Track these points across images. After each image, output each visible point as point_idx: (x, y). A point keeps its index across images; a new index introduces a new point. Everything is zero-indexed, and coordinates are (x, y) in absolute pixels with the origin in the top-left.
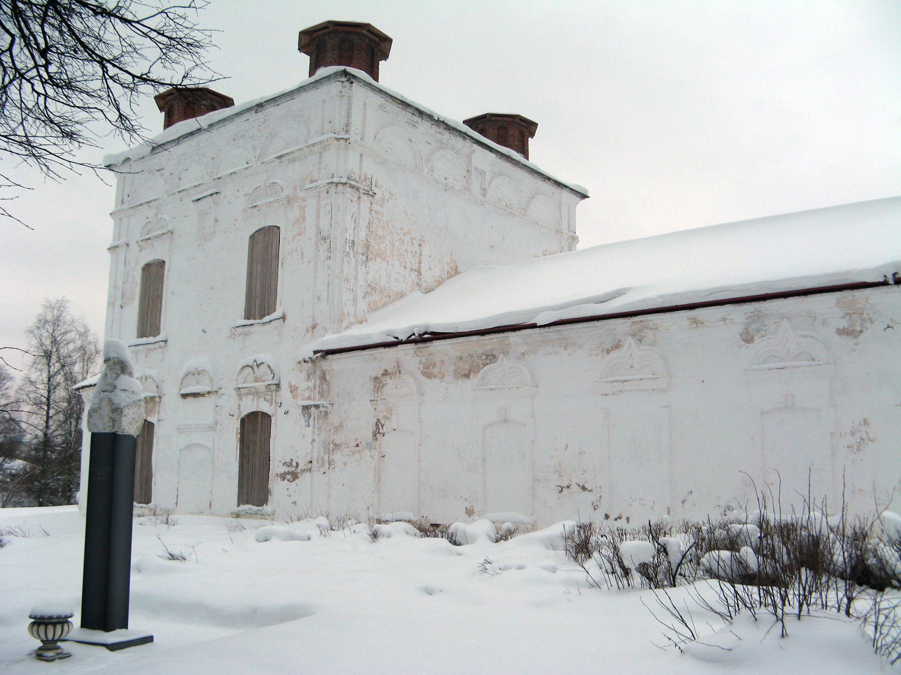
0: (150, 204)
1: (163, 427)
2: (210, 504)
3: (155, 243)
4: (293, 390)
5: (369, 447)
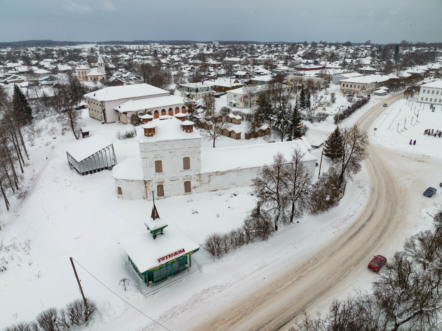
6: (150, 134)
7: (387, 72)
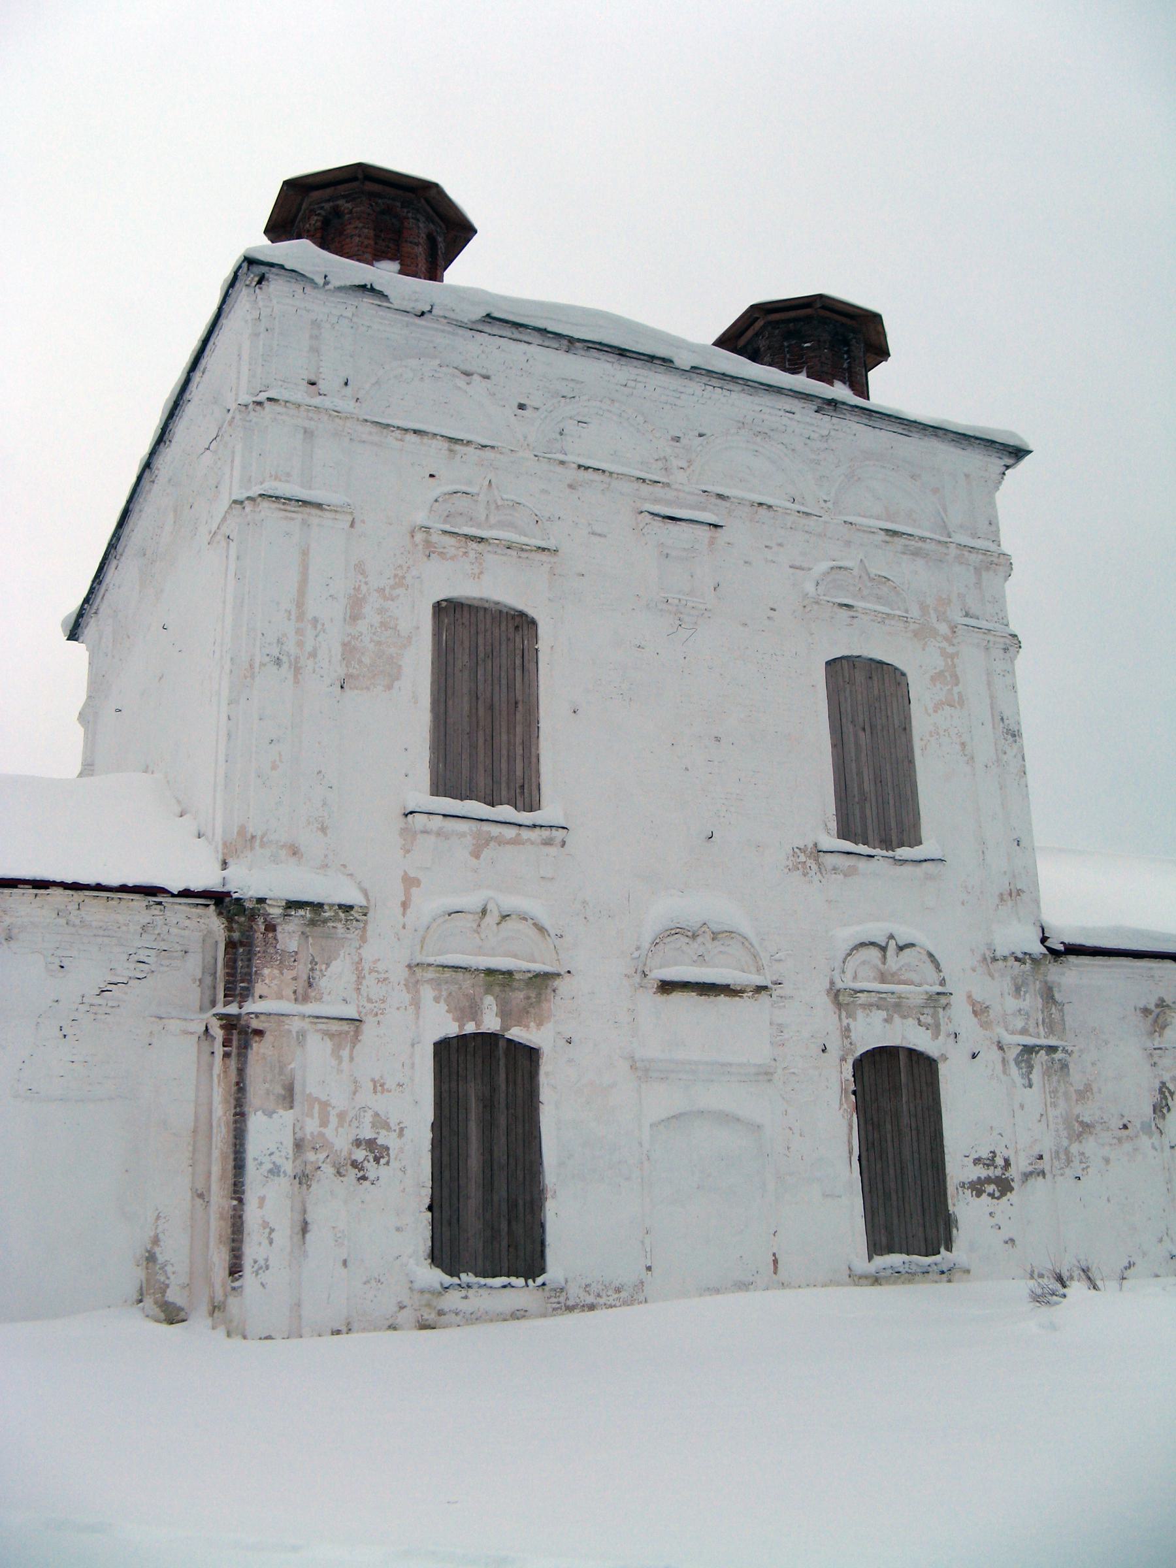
0: (458, 447)
2: (775, 1262)
3: (489, 557)
4: (979, 1010)
5: (1146, 1129)
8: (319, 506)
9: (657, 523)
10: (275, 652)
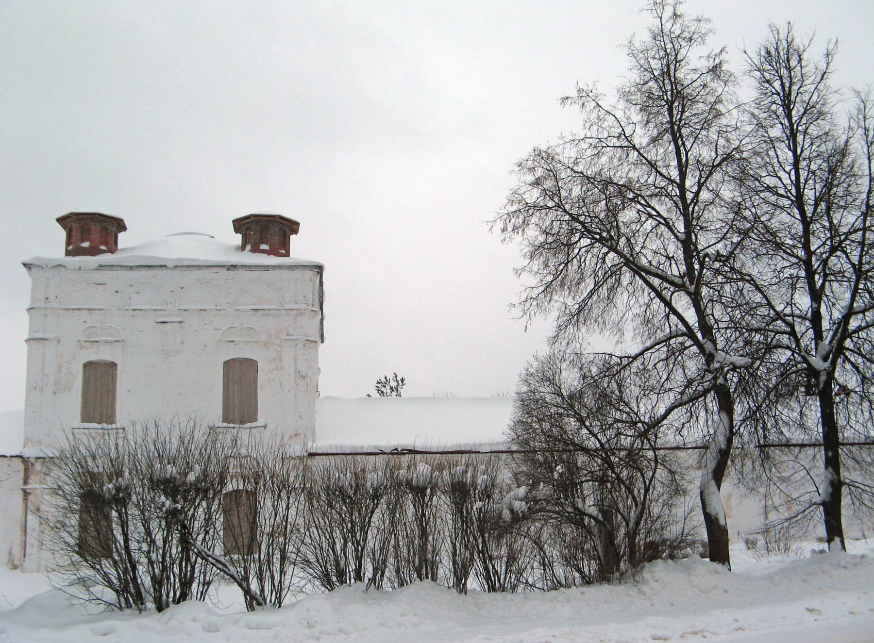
0: (92, 312)
1: (859, 598)
6: (86, 244)
7: (728, 157)
8: (46, 339)
9: (159, 325)
10: (35, 386)
